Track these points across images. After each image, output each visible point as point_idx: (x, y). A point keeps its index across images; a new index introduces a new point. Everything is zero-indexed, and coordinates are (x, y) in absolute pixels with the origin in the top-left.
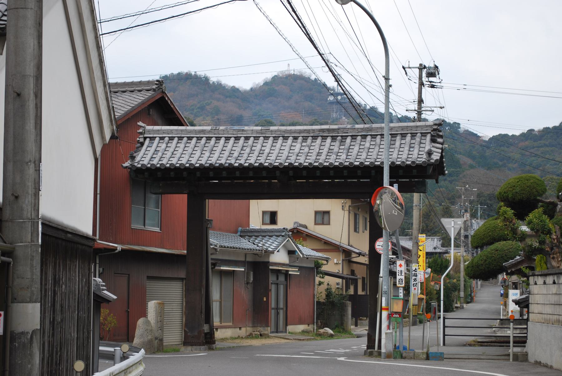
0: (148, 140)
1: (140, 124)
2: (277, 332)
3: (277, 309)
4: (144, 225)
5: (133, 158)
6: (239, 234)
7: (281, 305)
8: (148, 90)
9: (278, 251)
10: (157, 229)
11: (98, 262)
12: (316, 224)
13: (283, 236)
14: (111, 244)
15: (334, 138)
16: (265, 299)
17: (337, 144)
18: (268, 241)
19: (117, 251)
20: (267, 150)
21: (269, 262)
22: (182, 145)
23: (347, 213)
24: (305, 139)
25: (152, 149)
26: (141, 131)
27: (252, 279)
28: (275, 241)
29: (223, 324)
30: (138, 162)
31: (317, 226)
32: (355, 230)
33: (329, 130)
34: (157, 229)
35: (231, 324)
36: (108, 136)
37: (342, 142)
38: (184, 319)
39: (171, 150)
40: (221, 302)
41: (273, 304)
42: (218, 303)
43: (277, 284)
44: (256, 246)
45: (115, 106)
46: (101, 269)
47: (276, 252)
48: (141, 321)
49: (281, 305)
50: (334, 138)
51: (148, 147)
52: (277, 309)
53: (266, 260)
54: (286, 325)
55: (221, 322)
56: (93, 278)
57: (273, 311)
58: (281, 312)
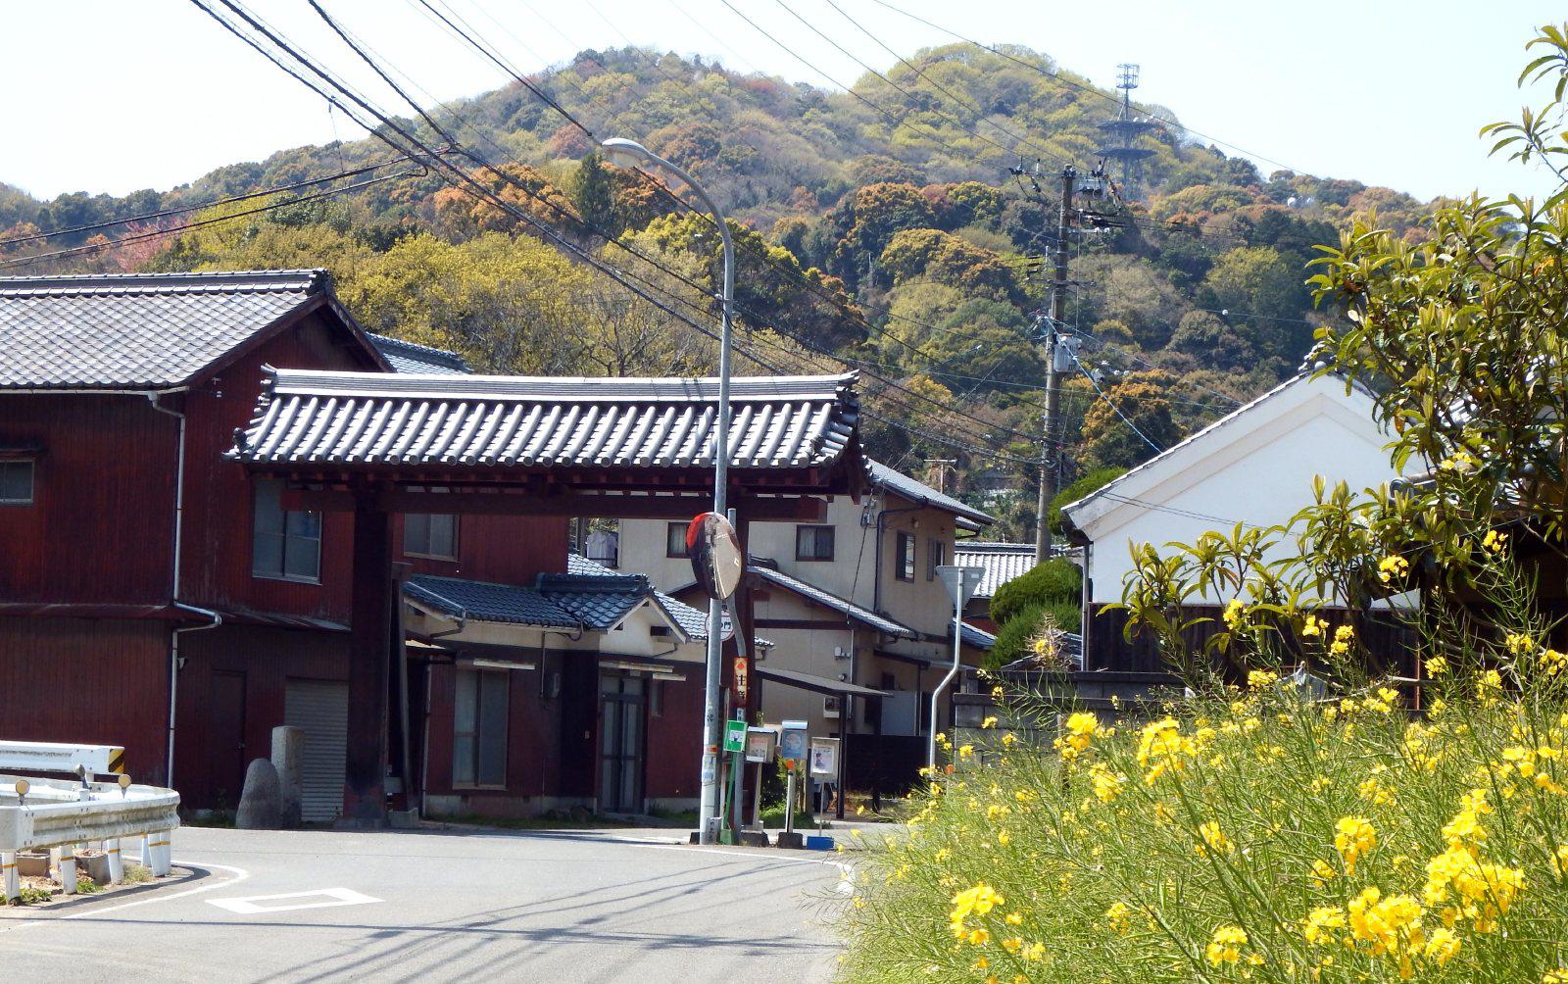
1: (267, 368)
2: (616, 810)
3: (618, 758)
4: (283, 571)
5: (242, 440)
6: (538, 586)
7: (631, 748)
8: (294, 291)
9: (619, 628)
10: (314, 580)
11: (175, 644)
12: (798, 558)
13: (634, 594)
14: (202, 611)
16: (587, 736)
18: (599, 604)
19: (212, 626)
23: (872, 534)
26: (267, 382)
27: (556, 691)
28: (615, 605)
29: (482, 787)
31: (801, 564)
32: (900, 574)
33: (669, 389)
35: (501, 787)
40: (476, 738)
41: (608, 747)
42: (470, 740)
43: (621, 703)
46: (182, 661)
47: (611, 630)
48: (253, 768)
49: (631, 748)
52: (618, 758)
53: (592, 648)
54: (643, 795)
55: (476, 780)
56: (1081, 638)
57: (607, 764)
58: (630, 768)
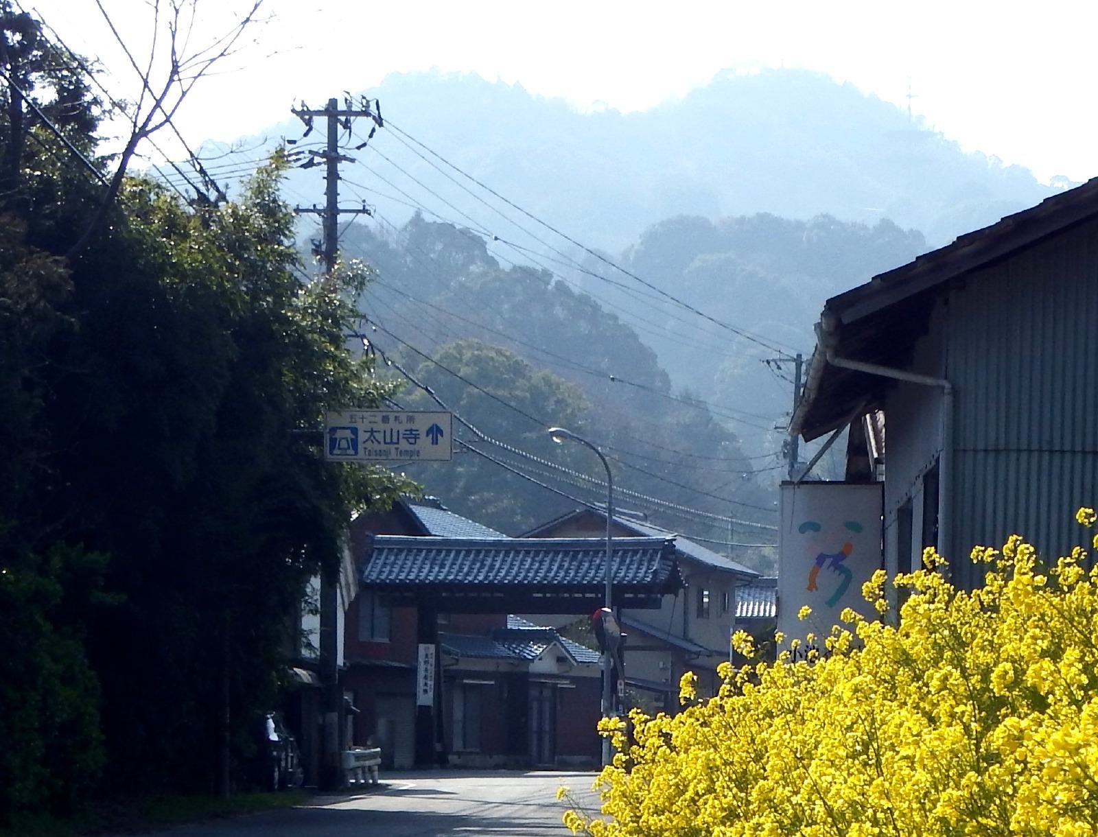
0: (376, 551)
10: (386, 640)
15: (566, 554)
17: (568, 559)
20: (498, 565)
21: (528, 673)
22: (411, 558)
24: (537, 553)
25: (380, 562)
30: (367, 577)
34: (386, 640)
35: (478, 750)
36: (353, 595)
37: (574, 558)
38: (369, 569)
39: (400, 563)
41: (534, 724)
44: (511, 653)
45: (212, 178)
49: (547, 727)
50: (566, 554)
51: (376, 559)
52: (540, 731)
53: (525, 670)
58: (547, 738)
